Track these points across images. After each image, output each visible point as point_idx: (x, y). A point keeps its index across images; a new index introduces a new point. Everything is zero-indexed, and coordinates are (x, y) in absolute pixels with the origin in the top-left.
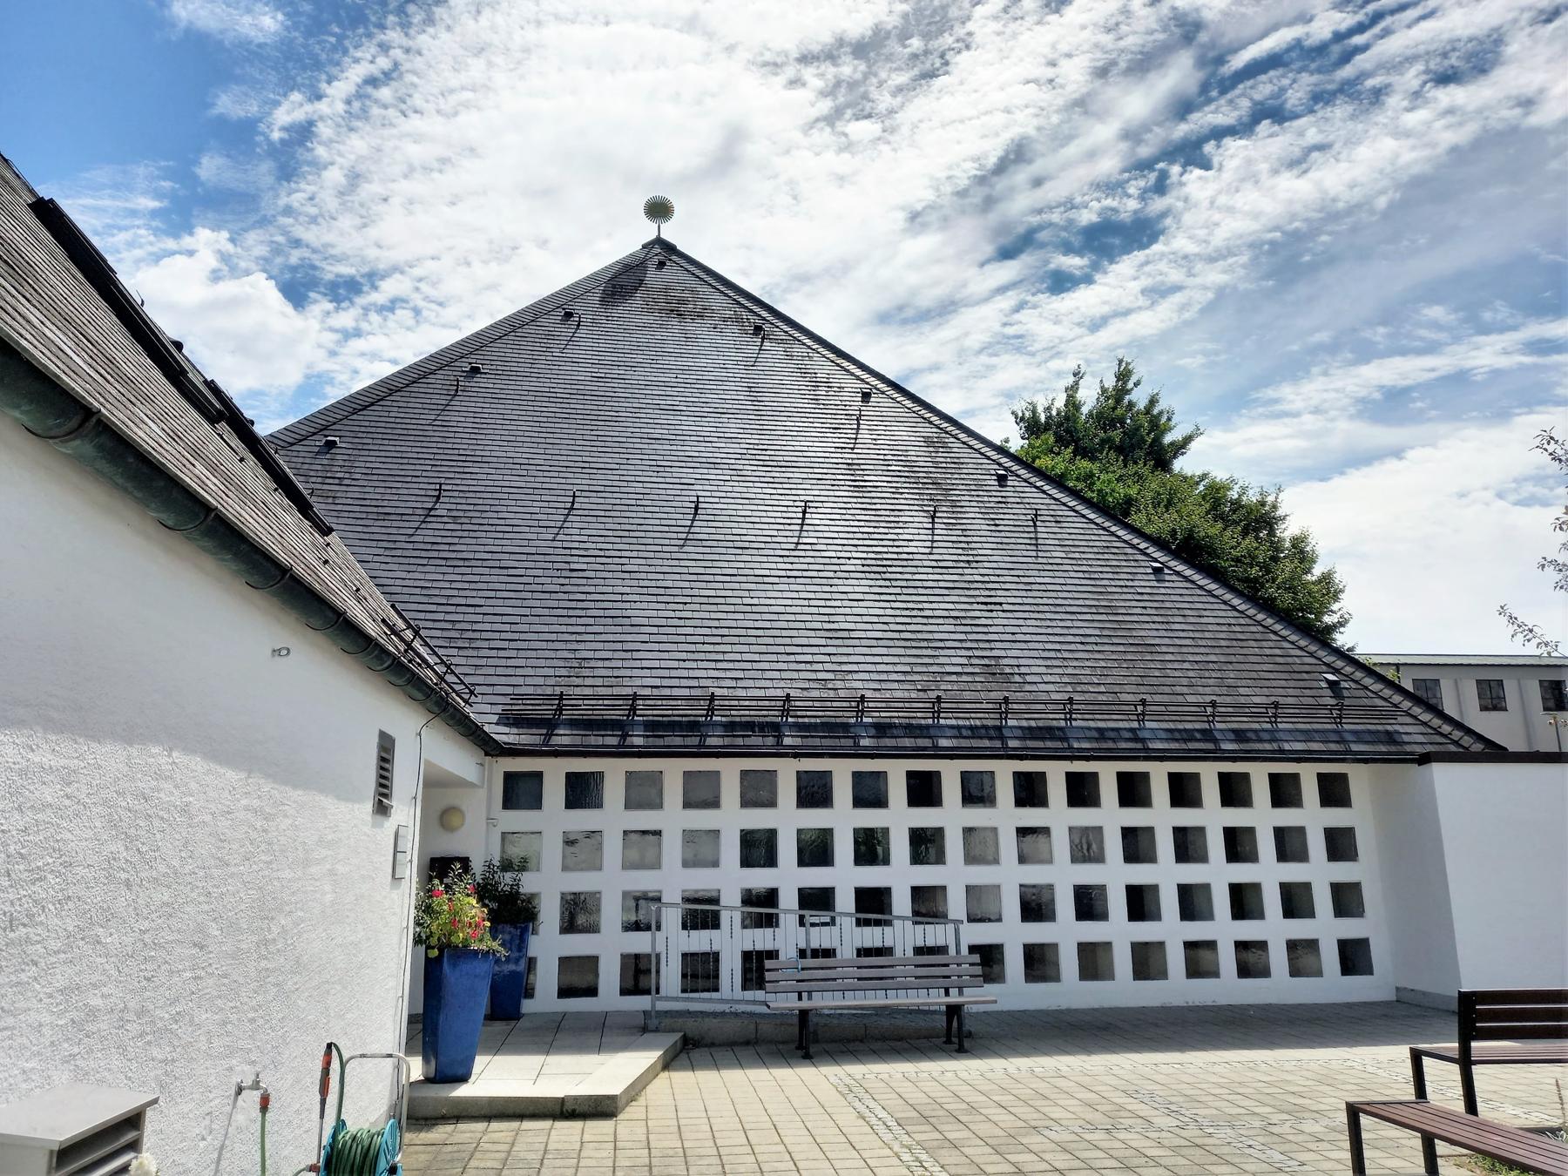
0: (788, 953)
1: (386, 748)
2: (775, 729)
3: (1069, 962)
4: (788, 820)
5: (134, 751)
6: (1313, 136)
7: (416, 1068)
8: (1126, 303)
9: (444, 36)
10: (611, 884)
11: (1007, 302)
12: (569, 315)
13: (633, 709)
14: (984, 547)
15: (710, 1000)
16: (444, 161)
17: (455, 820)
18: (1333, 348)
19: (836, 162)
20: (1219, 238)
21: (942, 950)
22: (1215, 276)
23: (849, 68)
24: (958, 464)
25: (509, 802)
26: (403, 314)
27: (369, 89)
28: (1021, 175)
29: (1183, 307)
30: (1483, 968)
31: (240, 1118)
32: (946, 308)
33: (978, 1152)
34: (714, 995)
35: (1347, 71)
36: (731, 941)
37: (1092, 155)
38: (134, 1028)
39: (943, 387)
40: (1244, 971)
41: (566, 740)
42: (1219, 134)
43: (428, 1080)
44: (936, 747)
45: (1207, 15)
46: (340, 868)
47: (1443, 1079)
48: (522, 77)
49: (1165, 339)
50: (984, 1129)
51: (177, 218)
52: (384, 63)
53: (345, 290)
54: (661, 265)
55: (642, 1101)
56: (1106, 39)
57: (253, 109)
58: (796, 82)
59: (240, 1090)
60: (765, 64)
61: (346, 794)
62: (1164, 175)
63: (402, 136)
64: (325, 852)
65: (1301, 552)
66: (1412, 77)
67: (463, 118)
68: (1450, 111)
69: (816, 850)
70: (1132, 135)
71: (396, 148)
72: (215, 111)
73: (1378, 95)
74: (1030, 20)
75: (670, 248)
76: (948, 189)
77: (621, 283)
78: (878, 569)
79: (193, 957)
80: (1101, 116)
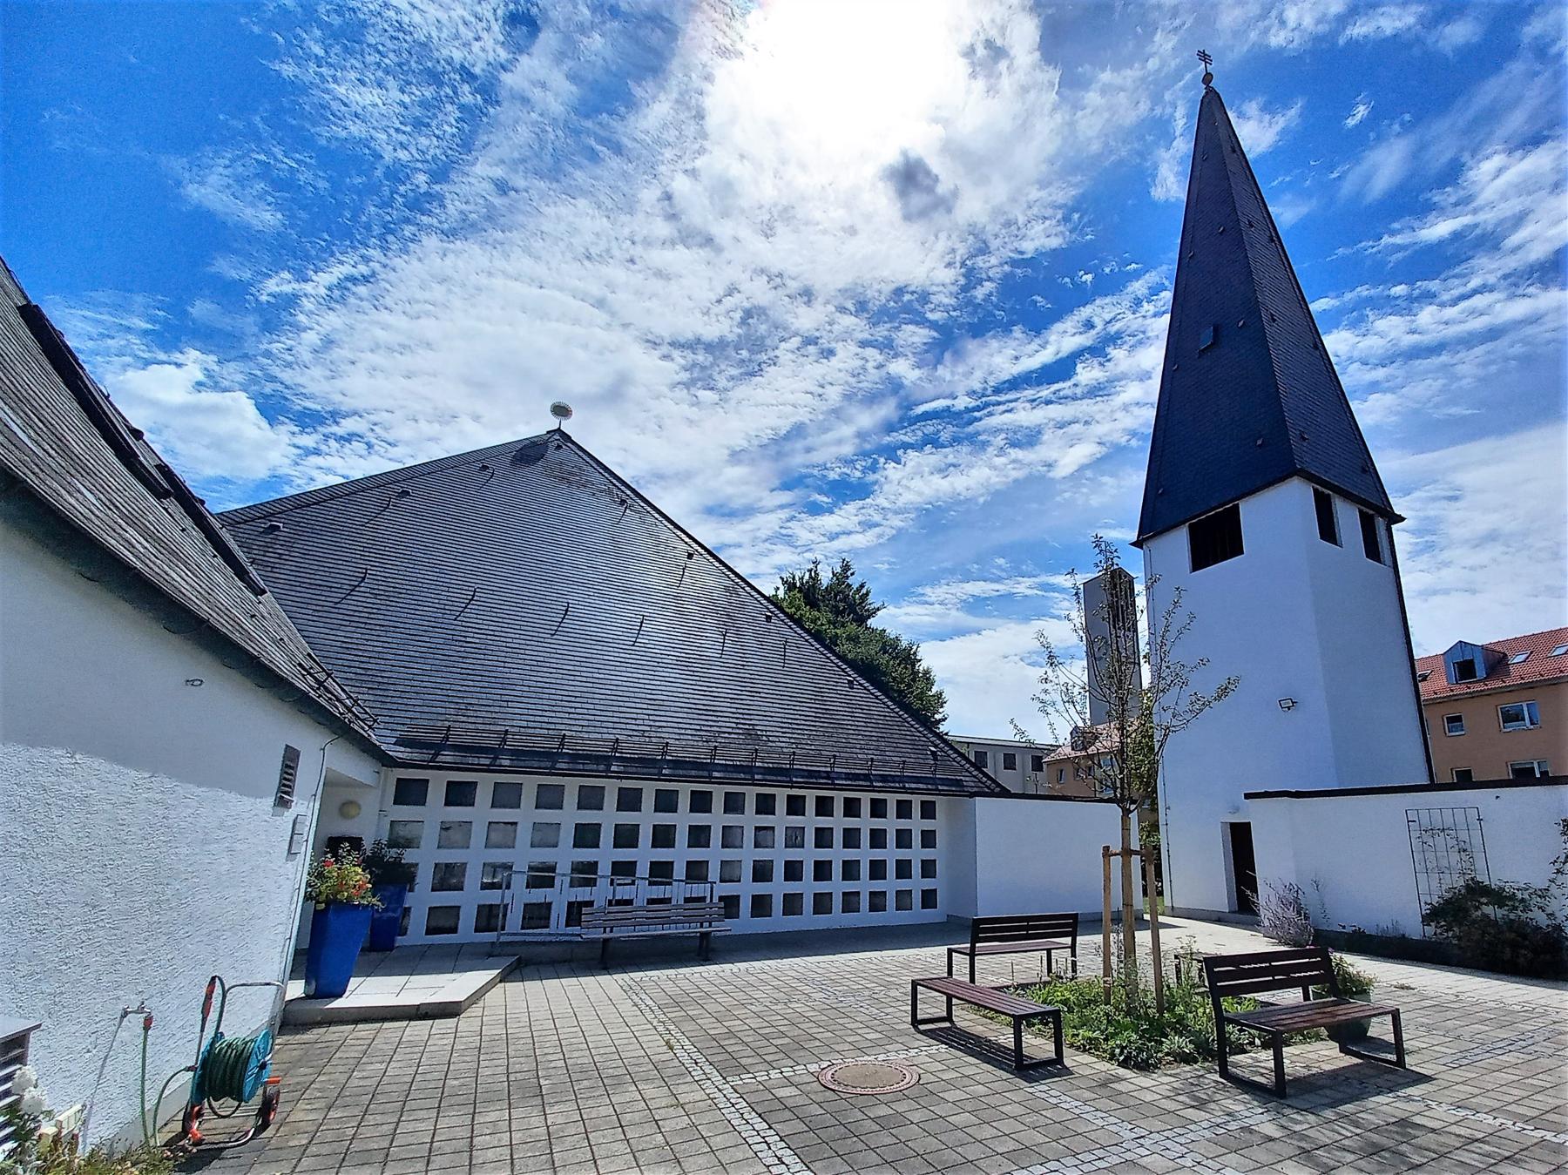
0: (600, 902)
1: (291, 759)
3: (778, 905)
4: (609, 817)
5: (36, 752)
6: (951, 459)
8: (850, 527)
9: (415, 262)
10: (475, 858)
11: (784, 514)
12: (485, 468)
13: (504, 740)
16: (404, 346)
17: (353, 811)
18: (952, 572)
20: (901, 502)
22: (897, 522)
23: (701, 357)
24: (743, 604)
26: (359, 446)
27: (349, 285)
28: (799, 445)
29: (880, 536)
31: (123, 1035)
32: (748, 512)
33: (707, 1022)
35: (970, 429)
36: (560, 896)
37: (840, 442)
38: (24, 970)
39: (742, 558)
40: (874, 908)
41: (449, 759)
42: (906, 446)
43: (308, 997)
45: (906, 382)
46: (238, 846)
47: (961, 961)
48: (473, 306)
49: (868, 551)
50: (711, 1007)
51: (170, 337)
52: (363, 269)
53: (308, 420)
54: (559, 447)
55: (481, 1004)
56: (852, 380)
57: (247, 275)
58: (666, 357)
59: (125, 1014)
60: (648, 341)
62: (876, 462)
64: (223, 834)
65: (927, 678)
66: (999, 440)
67: (423, 322)
68: (1014, 461)
69: (626, 837)
70: (861, 435)
71: (366, 330)
72: (213, 270)
73: (985, 444)
74: (811, 359)
75: (567, 438)
76: (756, 442)
77: (528, 453)
78: (684, 664)
80: (848, 421)
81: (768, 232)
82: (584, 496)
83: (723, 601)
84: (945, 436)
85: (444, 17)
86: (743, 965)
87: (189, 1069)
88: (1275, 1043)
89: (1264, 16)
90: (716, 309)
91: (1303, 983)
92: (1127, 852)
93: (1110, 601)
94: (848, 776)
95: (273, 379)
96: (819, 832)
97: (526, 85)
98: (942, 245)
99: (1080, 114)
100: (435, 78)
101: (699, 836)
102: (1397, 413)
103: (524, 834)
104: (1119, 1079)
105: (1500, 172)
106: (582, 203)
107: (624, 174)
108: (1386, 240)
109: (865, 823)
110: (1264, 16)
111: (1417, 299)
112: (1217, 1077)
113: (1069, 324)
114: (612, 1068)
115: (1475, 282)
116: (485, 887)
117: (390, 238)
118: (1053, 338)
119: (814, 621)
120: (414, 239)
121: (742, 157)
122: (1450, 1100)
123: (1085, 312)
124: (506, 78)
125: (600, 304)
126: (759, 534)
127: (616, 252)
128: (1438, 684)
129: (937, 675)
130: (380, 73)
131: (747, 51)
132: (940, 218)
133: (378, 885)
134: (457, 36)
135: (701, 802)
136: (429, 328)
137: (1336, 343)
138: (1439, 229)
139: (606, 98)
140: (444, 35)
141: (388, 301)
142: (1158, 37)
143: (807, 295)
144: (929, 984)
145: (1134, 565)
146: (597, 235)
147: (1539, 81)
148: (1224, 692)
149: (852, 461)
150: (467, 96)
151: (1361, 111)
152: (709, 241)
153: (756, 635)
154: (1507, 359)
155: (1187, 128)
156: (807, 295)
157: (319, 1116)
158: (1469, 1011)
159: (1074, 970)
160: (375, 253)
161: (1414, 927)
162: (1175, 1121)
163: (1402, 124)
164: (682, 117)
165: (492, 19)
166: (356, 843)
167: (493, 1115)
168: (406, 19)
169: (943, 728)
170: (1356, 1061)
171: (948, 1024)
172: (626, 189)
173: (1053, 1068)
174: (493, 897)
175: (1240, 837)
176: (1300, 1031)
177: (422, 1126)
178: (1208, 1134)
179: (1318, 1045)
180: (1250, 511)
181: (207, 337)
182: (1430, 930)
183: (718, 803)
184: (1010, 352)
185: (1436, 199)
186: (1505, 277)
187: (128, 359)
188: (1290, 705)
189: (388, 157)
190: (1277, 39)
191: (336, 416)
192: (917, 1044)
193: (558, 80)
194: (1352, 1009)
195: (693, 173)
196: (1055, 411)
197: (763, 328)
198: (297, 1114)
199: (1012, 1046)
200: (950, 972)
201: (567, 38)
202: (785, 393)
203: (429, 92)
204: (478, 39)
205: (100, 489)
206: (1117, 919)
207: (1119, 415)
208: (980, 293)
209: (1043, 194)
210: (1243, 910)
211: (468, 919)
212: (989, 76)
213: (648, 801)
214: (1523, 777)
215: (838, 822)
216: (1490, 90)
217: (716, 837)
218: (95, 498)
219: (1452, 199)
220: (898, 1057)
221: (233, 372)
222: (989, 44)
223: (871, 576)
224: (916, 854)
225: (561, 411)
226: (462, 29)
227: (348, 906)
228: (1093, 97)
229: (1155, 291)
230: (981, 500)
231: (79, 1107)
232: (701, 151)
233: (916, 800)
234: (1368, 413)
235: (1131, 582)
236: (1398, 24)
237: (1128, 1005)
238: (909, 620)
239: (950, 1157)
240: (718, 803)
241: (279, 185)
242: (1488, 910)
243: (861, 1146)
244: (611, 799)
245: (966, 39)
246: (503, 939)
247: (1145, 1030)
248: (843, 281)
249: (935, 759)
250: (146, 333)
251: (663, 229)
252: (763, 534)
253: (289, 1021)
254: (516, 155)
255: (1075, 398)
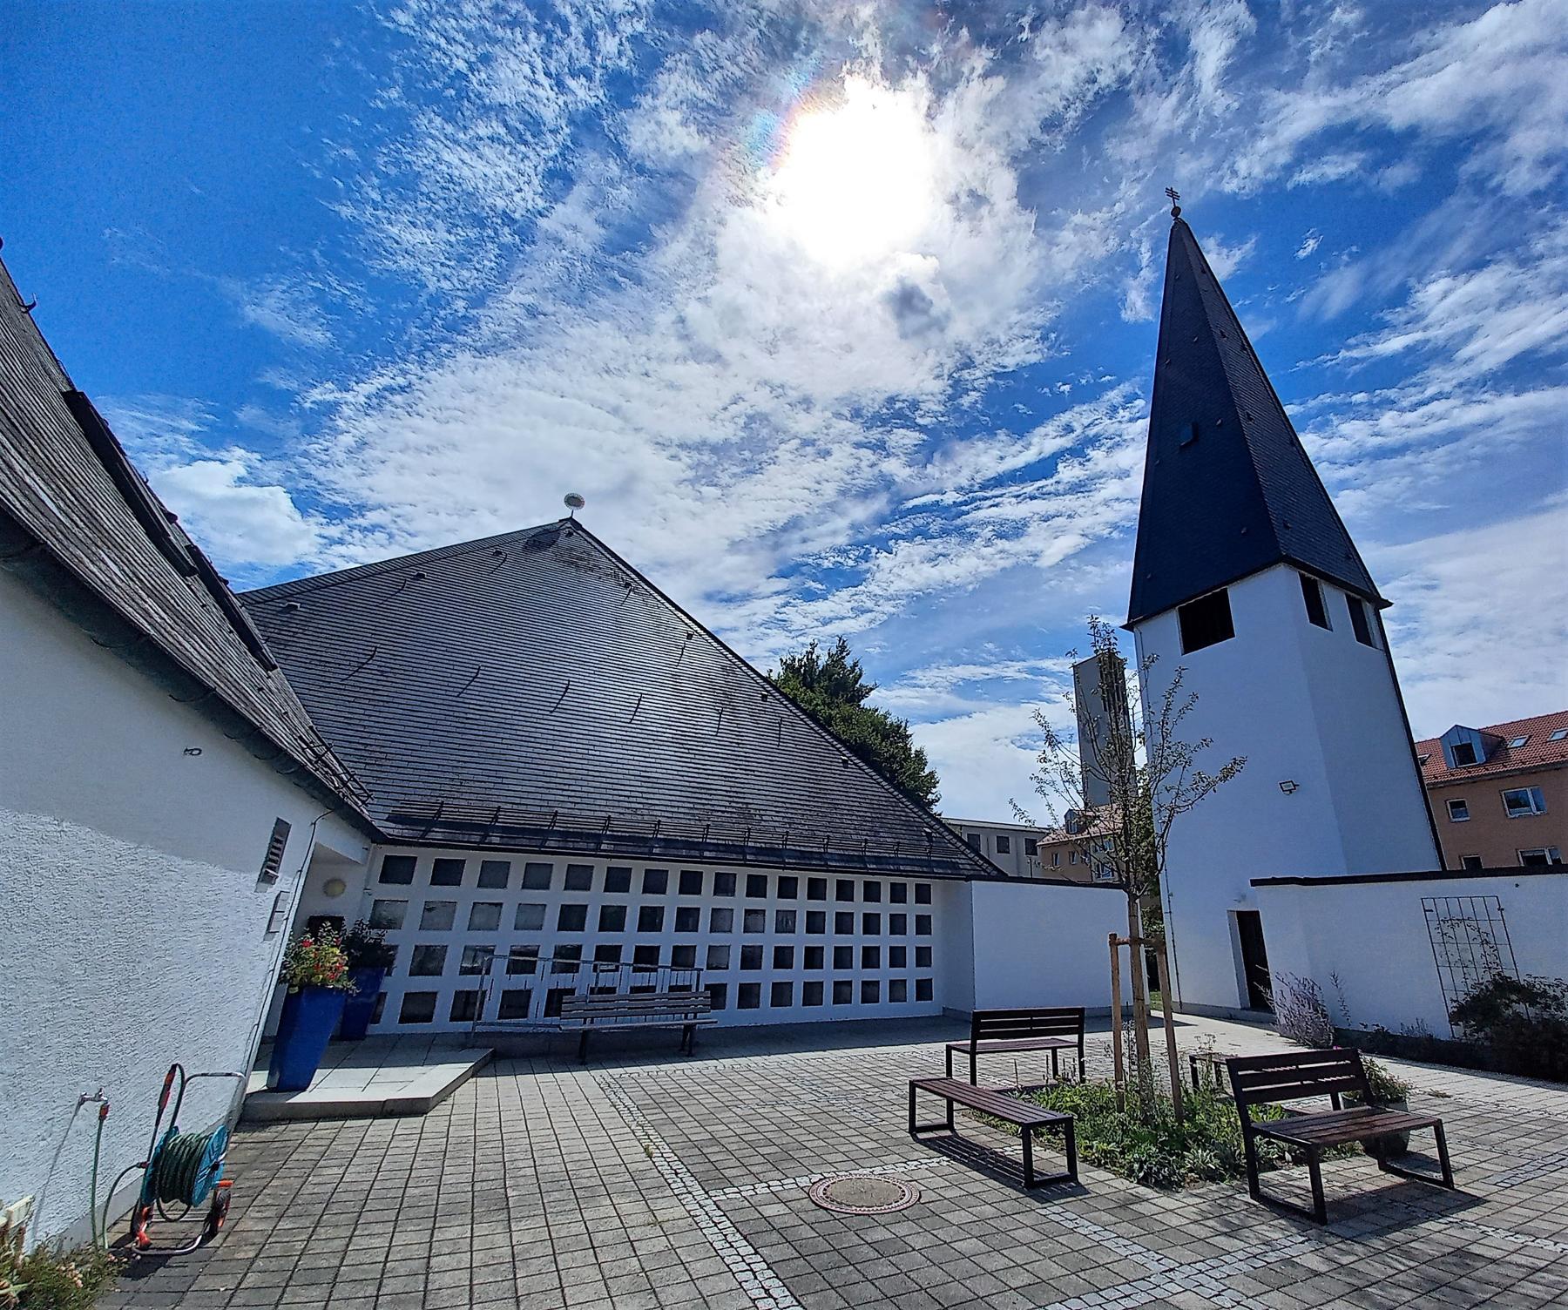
2: (598, 839)
6: (940, 549)
7: (259, 1081)
8: (843, 613)
9: (450, 377)
10: (456, 940)
13: (496, 818)
14: (748, 738)
15: (518, 1025)
17: (338, 889)
18: (942, 656)
19: (690, 503)
20: (891, 591)
21: (688, 988)
22: (888, 608)
23: (706, 457)
25: (385, 878)
28: (796, 536)
30: (985, 1000)
31: (79, 1123)
32: (746, 597)
33: (689, 1126)
34: (522, 1020)
35: (958, 522)
36: (540, 983)
37: (834, 533)
41: (439, 836)
42: (897, 537)
43: (271, 1090)
44: (702, 857)
46: (217, 923)
47: (960, 1060)
49: (861, 635)
50: (692, 1110)
52: (401, 381)
53: (335, 513)
54: (570, 534)
55: (450, 1101)
56: (847, 478)
57: (294, 385)
58: (673, 457)
61: (234, 864)
63: (403, 427)
65: (920, 758)
66: (987, 532)
67: (452, 426)
69: (612, 919)
72: (261, 380)
74: (809, 458)
75: (577, 526)
76: (755, 533)
77: (540, 540)
78: (680, 741)
79: (52, 992)
80: (842, 514)
81: (771, 349)
82: (590, 579)
83: (720, 681)
84: (934, 528)
85: (488, 171)
86: (728, 1062)
87: (140, 1165)
88: (1310, 1157)
89: (1217, 168)
90: (721, 416)
91: (1332, 1089)
92: (1134, 941)
93: (1100, 684)
94: (842, 858)
95: (308, 476)
96: (682, 912)
97: (560, 228)
98: (931, 360)
99: (1055, 249)
100: (479, 222)
101: (687, 919)
102: (1368, 509)
103: (508, 915)
104: (1140, 1200)
105: (1445, 295)
106: (605, 325)
107: (643, 302)
108: (1343, 354)
109: (858, 907)
110: (1217, 168)
111: (1378, 405)
112: (1247, 1198)
113: (1050, 428)
114: (587, 1177)
115: (1431, 391)
116: (464, 971)
117: (428, 354)
118: (1035, 440)
119: (810, 702)
120: (449, 355)
121: (750, 287)
122: (1508, 1225)
123: (1065, 417)
124: (542, 222)
125: (615, 411)
126: (754, 619)
127: (632, 366)
128: (1438, 768)
129: (929, 757)
130: (430, 217)
131: (757, 200)
132: (934, 337)
133: (355, 966)
134: (501, 188)
135: (690, 884)
136: (456, 430)
137: (1310, 442)
138: (1394, 344)
139: (629, 240)
140: (489, 187)
141: (421, 408)
142: (1122, 186)
143: (807, 403)
144: (928, 1085)
145: (1126, 648)
146: (616, 352)
147: (1481, 211)
148: (1227, 774)
149: (845, 551)
150: (507, 236)
151: (1311, 244)
152: (718, 358)
153: (752, 714)
154: (1469, 459)
155: (1153, 261)
156: (807, 403)
157: (267, 1226)
158: (1514, 1123)
159: (1082, 1072)
160: (413, 368)
161: (1443, 1030)
162: (1207, 1251)
163: (1350, 255)
164: (697, 254)
165: (532, 174)
166: (337, 922)
167: (453, 1231)
168: (457, 173)
169: (935, 809)
170: (1399, 1180)
171: (948, 1133)
172: (644, 314)
173: (1064, 1186)
174: (471, 983)
175: (1249, 927)
176: (1333, 1145)
177: (376, 1242)
178: (1244, 1267)
179: (1355, 1161)
180: (1242, 598)
181: (250, 438)
182: (1459, 1030)
183: (708, 884)
184: (996, 453)
185: (1388, 318)
186: (1460, 385)
187: (173, 457)
188: (1291, 788)
189: (432, 288)
190: (1230, 186)
191: (362, 509)
192: (916, 1155)
193: (588, 224)
194: (1389, 1121)
195: (705, 301)
196: (1039, 506)
197: (764, 432)
198: (249, 1222)
199: (1020, 1158)
200: (949, 1072)
201: (599, 190)
202: (782, 490)
203: (472, 234)
204: (520, 191)
205: (124, 561)
206: (1127, 1015)
207: (1100, 509)
208: (966, 401)
209: (1023, 316)
210: (1255, 1005)
211: (444, 1006)
212: (971, 220)
213: (637, 881)
214: (1535, 865)
215: (830, 906)
216: (1432, 223)
217: (705, 920)
218: (118, 569)
219: (1404, 318)
220: (897, 1171)
221: (272, 470)
222: (972, 193)
223: (868, 657)
224: (911, 941)
225: (574, 501)
226: (506, 182)
227: (322, 989)
228: (1067, 236)
229: (1129, 399)
230: (970, 588)
231: (27, 1199)
232: (713, 282)
233: (911, 884)
234: (1346, 505)
235: (1122, 663)
236: (1341, 170)
237: (1143, 1112)
238: (900, 702)
239: (957, 1292)
240: (708, 884)
241: (330, 308)
242: (1521, 1008)
243: (856, 1277)
244: (599, 879)
245: (951, 188)
246: (478, 1029)
247: (1159, 1139)
248: (838, 392)
249: (930, 841)
250: (192, 434)
251: (675, 347)
252: (759, 618)
253: (249, 1116)
254: (547, 285)
255: (1057, 494)
